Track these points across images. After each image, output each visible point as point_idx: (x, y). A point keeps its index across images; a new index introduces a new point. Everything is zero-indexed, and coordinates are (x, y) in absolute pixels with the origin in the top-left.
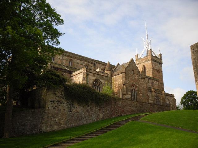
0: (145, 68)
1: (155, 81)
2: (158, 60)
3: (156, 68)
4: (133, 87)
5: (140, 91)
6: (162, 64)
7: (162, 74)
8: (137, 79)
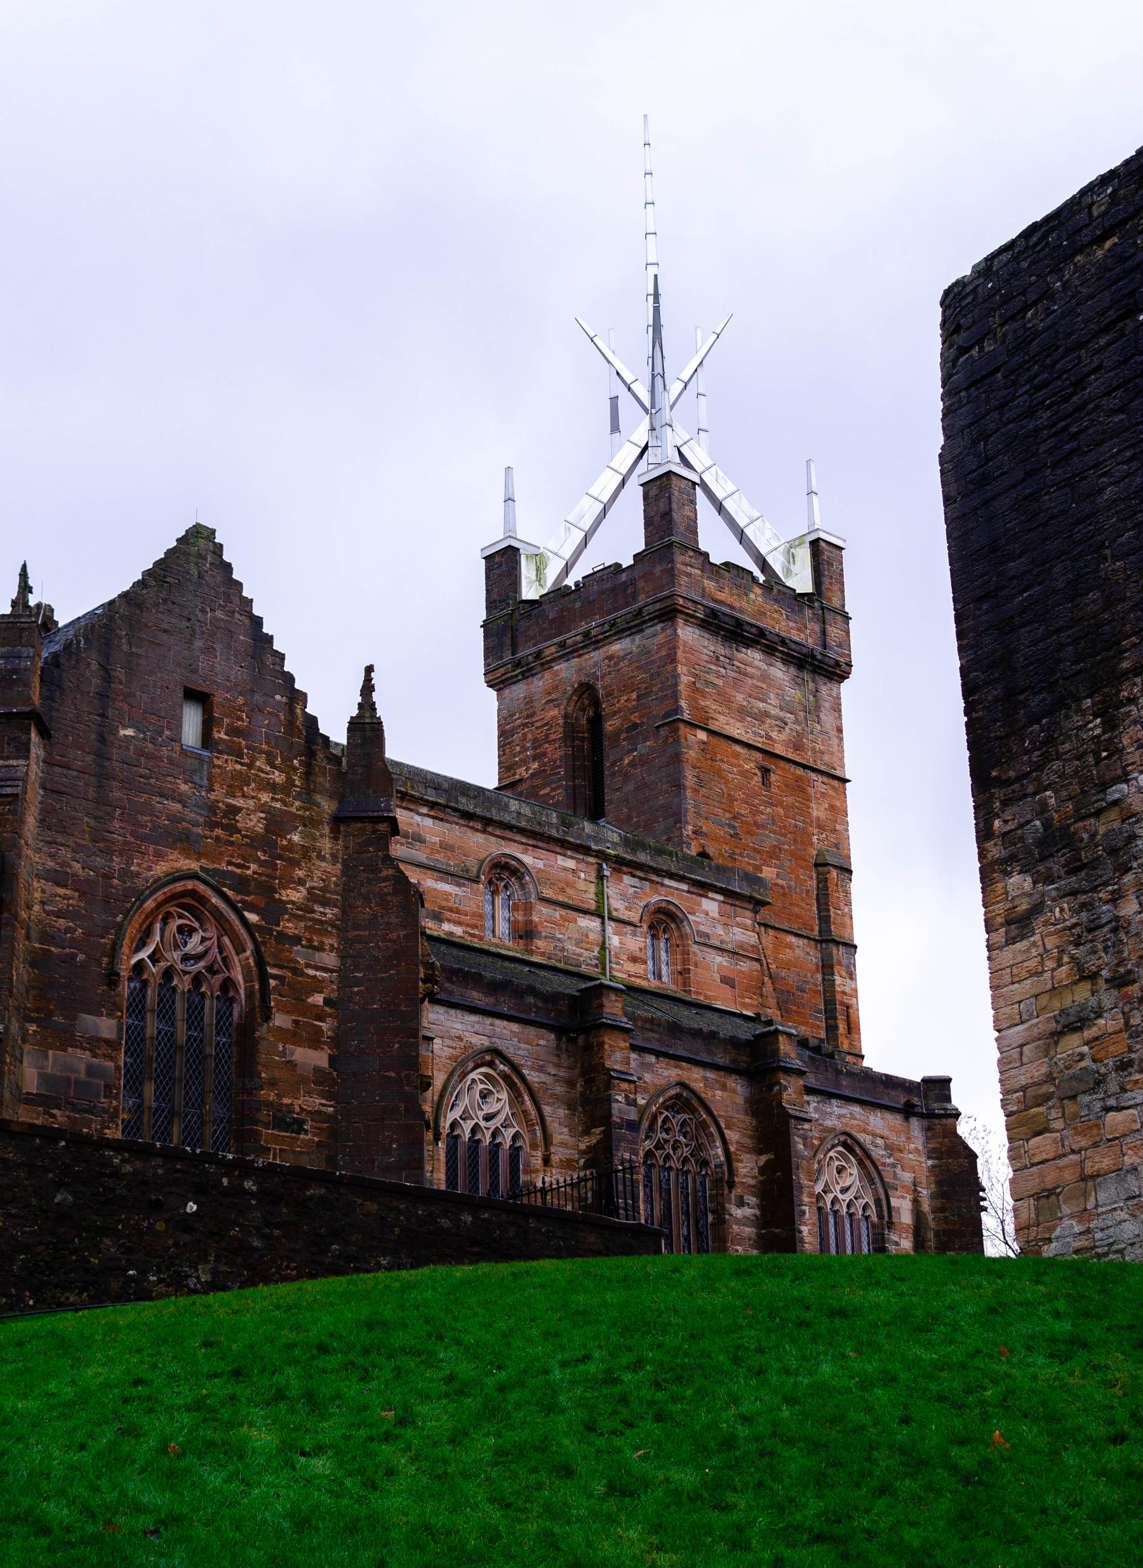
0: (596, 722)
1: (711, 905)
2: (780, 623)
3: (736, 730)
4: (186, 931)
5: (298, 1005)
6: (838, 671)
7: (839, 812)
8: (254, 823)
